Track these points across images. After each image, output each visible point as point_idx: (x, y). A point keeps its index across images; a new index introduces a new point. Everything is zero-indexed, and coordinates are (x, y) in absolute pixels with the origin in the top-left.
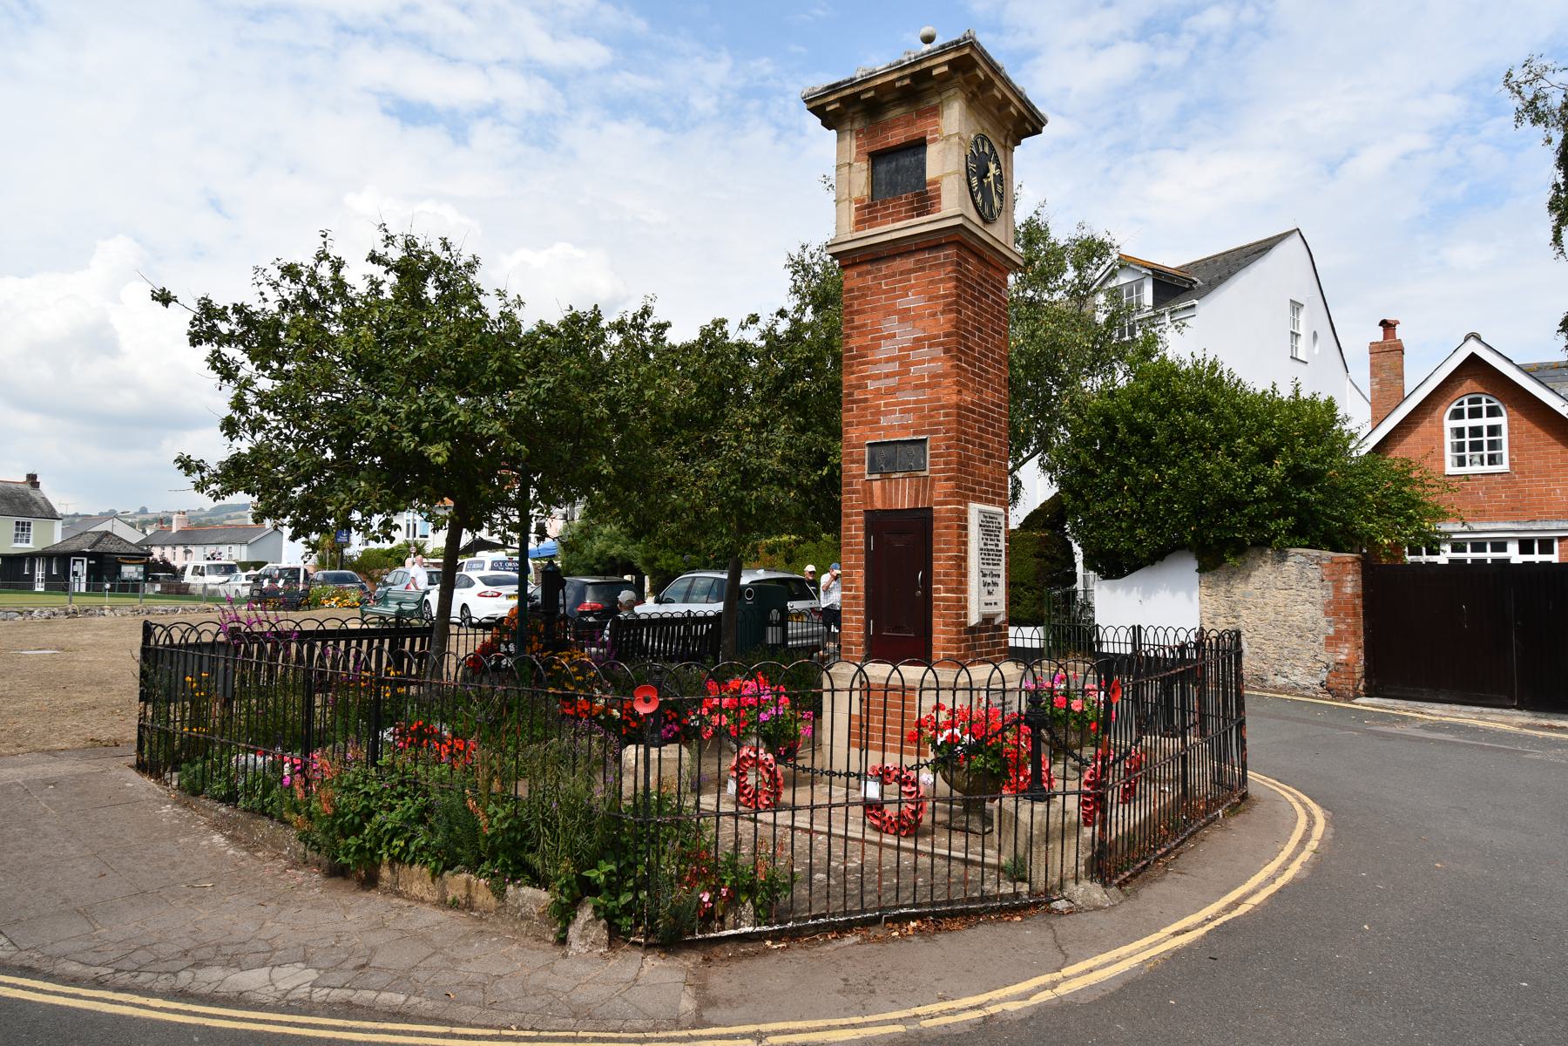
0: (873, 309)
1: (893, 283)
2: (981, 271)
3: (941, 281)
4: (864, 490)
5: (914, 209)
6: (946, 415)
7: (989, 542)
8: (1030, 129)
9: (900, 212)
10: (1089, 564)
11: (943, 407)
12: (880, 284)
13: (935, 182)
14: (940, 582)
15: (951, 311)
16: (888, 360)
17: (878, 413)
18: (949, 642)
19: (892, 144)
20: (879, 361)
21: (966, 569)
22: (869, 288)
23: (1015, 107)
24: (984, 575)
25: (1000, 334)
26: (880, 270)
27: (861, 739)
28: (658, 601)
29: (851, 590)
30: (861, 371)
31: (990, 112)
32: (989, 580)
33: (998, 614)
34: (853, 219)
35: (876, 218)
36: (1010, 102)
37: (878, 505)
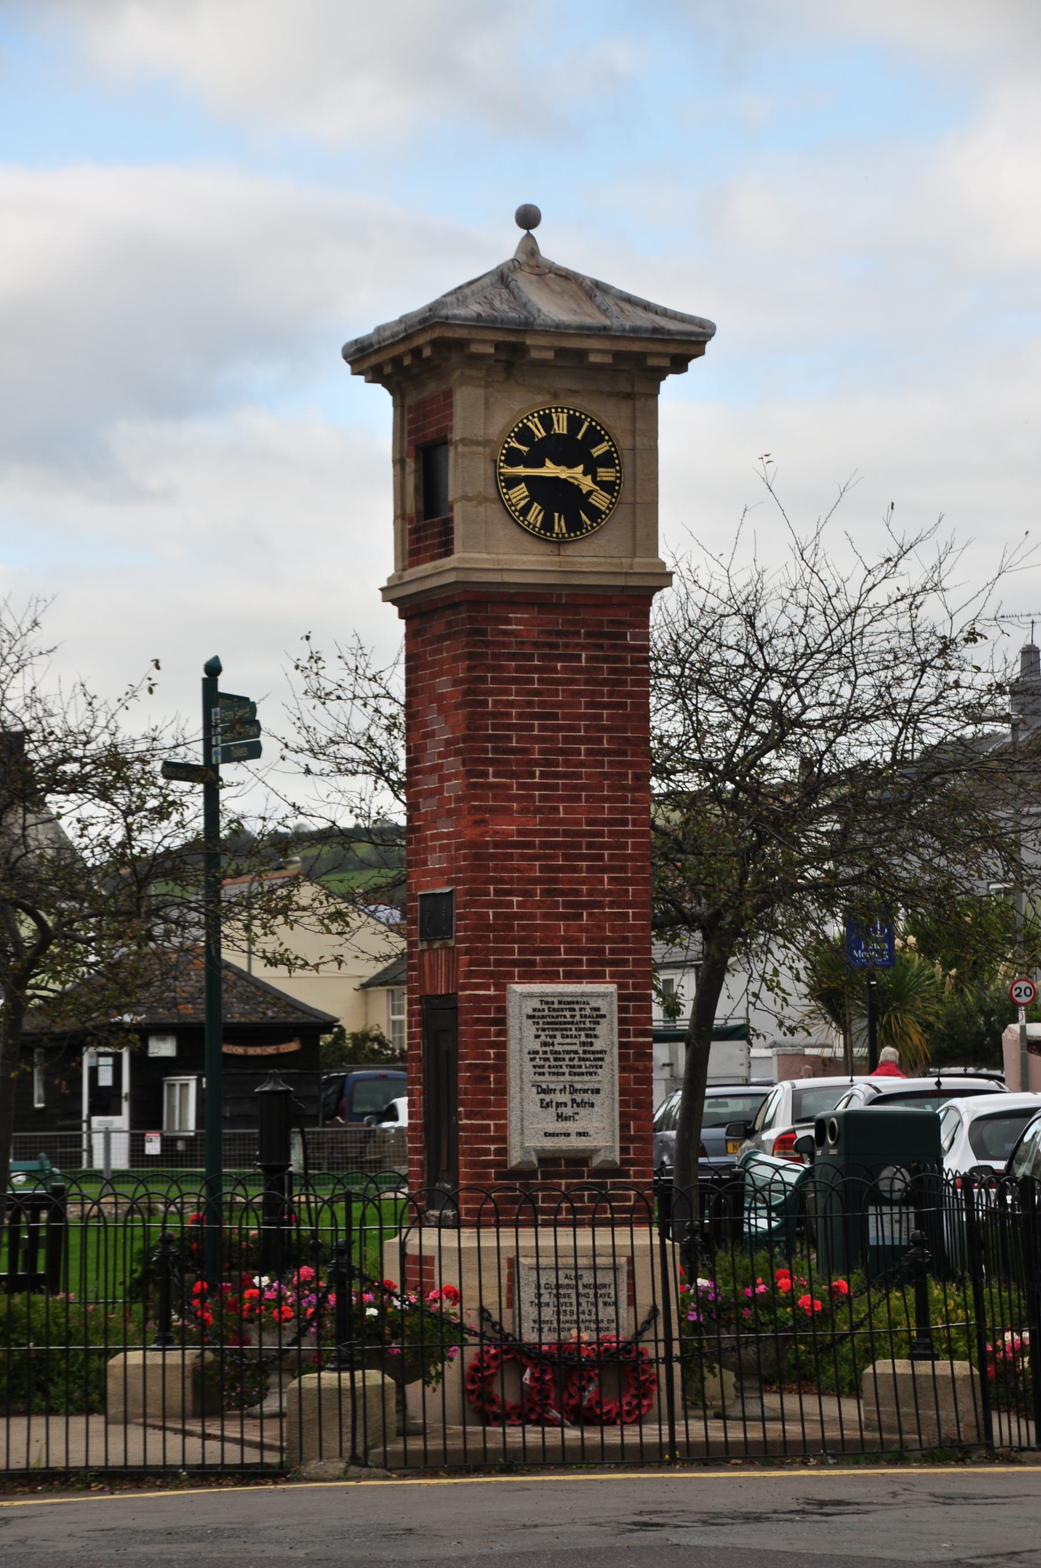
33: (595, 1151)
34: (407, 547)
37: (428, 991)
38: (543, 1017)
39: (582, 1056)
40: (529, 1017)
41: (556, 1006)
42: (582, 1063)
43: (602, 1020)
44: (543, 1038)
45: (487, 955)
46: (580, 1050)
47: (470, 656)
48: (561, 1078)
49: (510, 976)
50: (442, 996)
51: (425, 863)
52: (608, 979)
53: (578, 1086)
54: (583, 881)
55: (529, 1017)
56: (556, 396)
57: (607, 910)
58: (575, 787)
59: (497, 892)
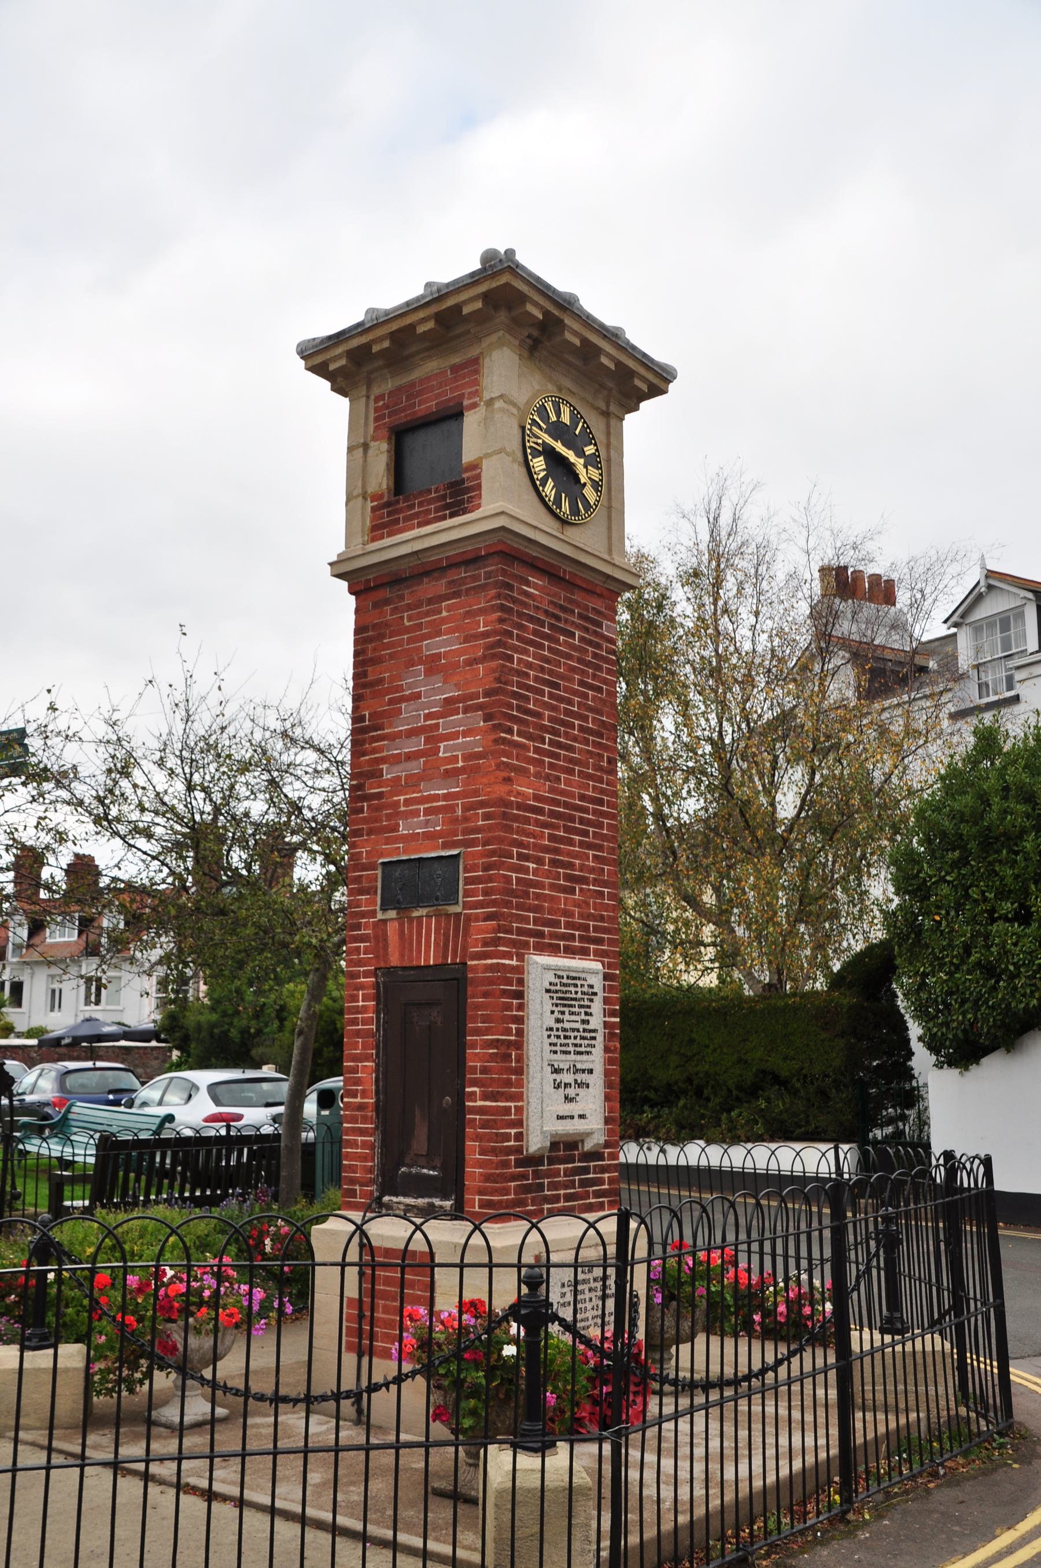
0: (392, 656)
1: (420, 616)
2: (555, 595)
3: (482, 611)
4: (376, 937)
5: (447, 506)
6: (487, 816)
7: (567, 1017)
8: (644, 388)
9: (428, 511)
10: (933, 1045)
11: (482, 804)
12: (402, 618)
13: (475, 466)
14: (475, 1083)
15: (494, 657)
16: (411, 733)
17: (397, 814)
18: (487, 1180)
19: (420, 414)
20: (398, 735)
21: (520, 1059)
22: (386, 625)
23: (608, 355)
24: (557, 1071)
25: (599, 690)
26: (402, 598)
27: (360, 1338)
28: (362, 1098)
29: (355, 1096)
30: (375, 751)
31: (569, 364)
32: (567, 1078)
33: (589, 1134)
34: (368, 523)
35: (397, 521)
36: (599, 351)
37: (394, 960)
38: (557, 992)
39: (582, 1034)
40: (548, 991)
41: (565, 981)
42: (582, 1042)
43: (595, 998)
44: (556, 1013)
45: (511, 922)
46: (581, 1027)
47: (502, 608)
48: (568, 1057)
49: (526, 945)
50: (419, 967)
51: (396, 828)
52: (592, 957)
53: (579, 1066)
54: (576, 855)
55: (548, 991)
56: (560, 389)
57: (591, 887)
58: (571, 760)
59: (519, 855)
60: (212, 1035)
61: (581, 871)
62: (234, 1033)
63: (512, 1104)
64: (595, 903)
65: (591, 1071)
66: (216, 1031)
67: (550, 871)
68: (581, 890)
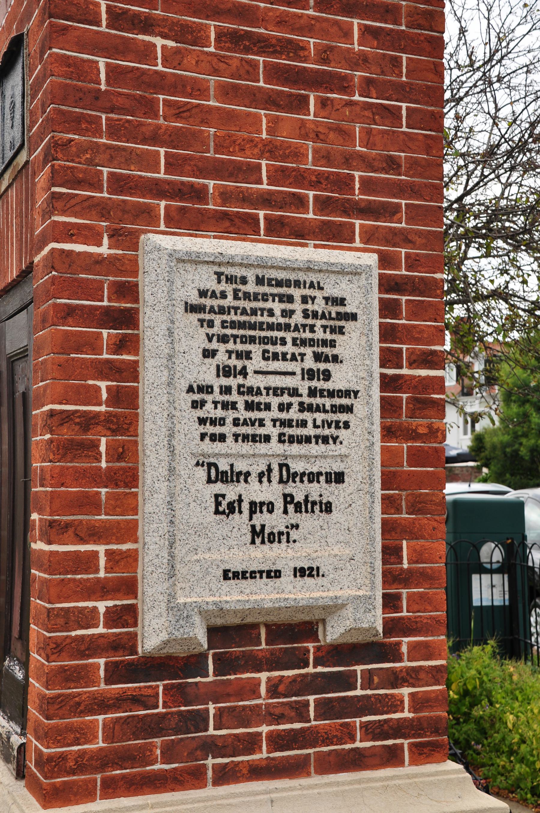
39: (306, 400)
40: (192, 308)
41: (251, 287)
42: (307, 416)
46: (304, 387)
53: (297, 466)
55: (192, 308)
57: (357, 98)
60: (505, 453)
61: (325, 61)
62: (523, 451)
63: (101, 549)
64: (369, 132)
65: (339, 478)
66: (508, 450)
67: (221, 59)
68: (323, 103)
